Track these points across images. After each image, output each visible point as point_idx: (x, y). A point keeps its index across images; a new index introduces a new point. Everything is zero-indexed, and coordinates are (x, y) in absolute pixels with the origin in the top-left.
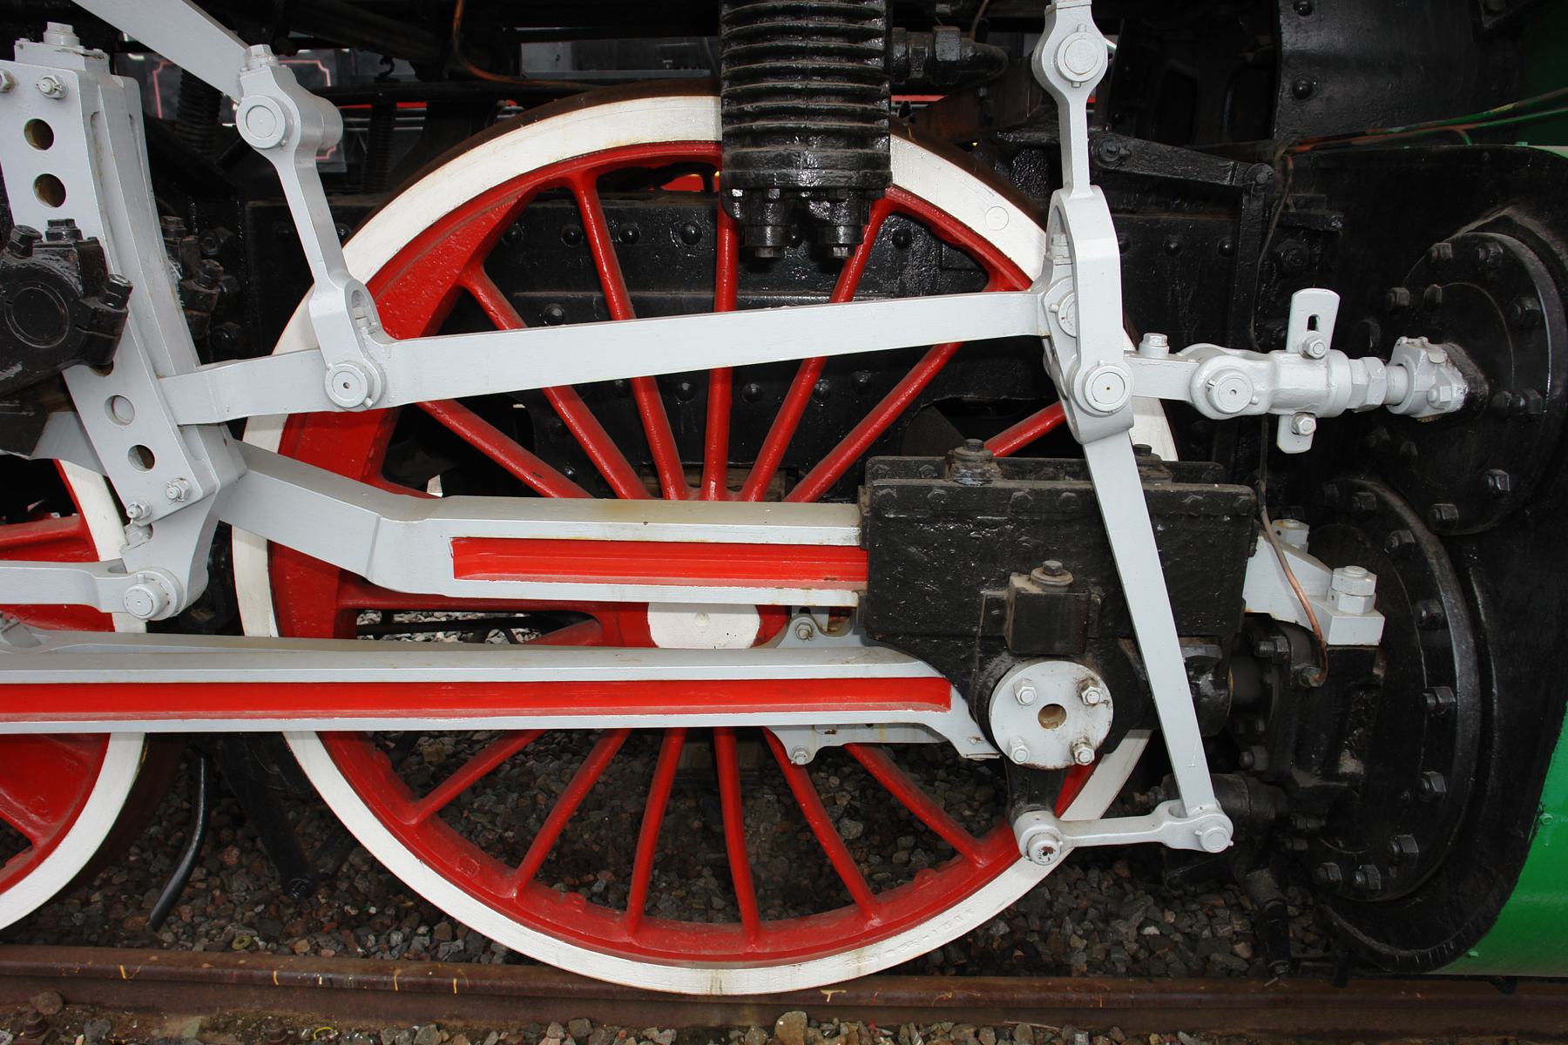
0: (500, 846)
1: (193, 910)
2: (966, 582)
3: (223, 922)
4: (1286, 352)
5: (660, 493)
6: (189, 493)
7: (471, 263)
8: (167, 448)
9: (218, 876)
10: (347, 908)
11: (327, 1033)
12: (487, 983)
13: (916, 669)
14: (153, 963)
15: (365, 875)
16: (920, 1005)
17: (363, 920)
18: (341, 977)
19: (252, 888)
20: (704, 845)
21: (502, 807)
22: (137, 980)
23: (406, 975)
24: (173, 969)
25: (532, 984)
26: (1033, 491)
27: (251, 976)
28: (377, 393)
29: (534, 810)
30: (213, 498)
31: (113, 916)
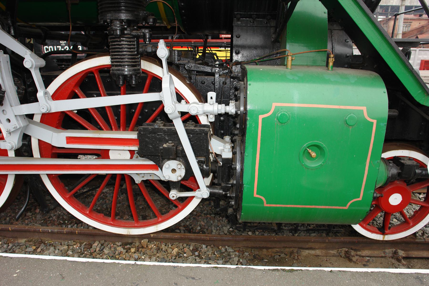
0: (96, 210)
1: (28, 221)
2: (157, 146)
3: (34, 223)
4: (181, 104)
5: (112, 129)
6: (16, 127)
7: (76, 86)
8: (13, 119)
9: (34, 215)
10: (61, 221)
11: (51, 242)
12: (83, 232)
13: (151, 163)
14: (16, 227)
15: (66, 215)
16: (171, 238)
17: (64, 223)
18: (54, 230)
19: (41, 217)
20: (142, 212)
21: (98, 203)
22: (13, 231)
23: (67, 230)
24: (20, 228)
25: (92, 232)
26: (167, 129)
27: (36, 230)
28: (49, 110)
29: (105, 204)
30: (21, 128)
31: (11, 222)
